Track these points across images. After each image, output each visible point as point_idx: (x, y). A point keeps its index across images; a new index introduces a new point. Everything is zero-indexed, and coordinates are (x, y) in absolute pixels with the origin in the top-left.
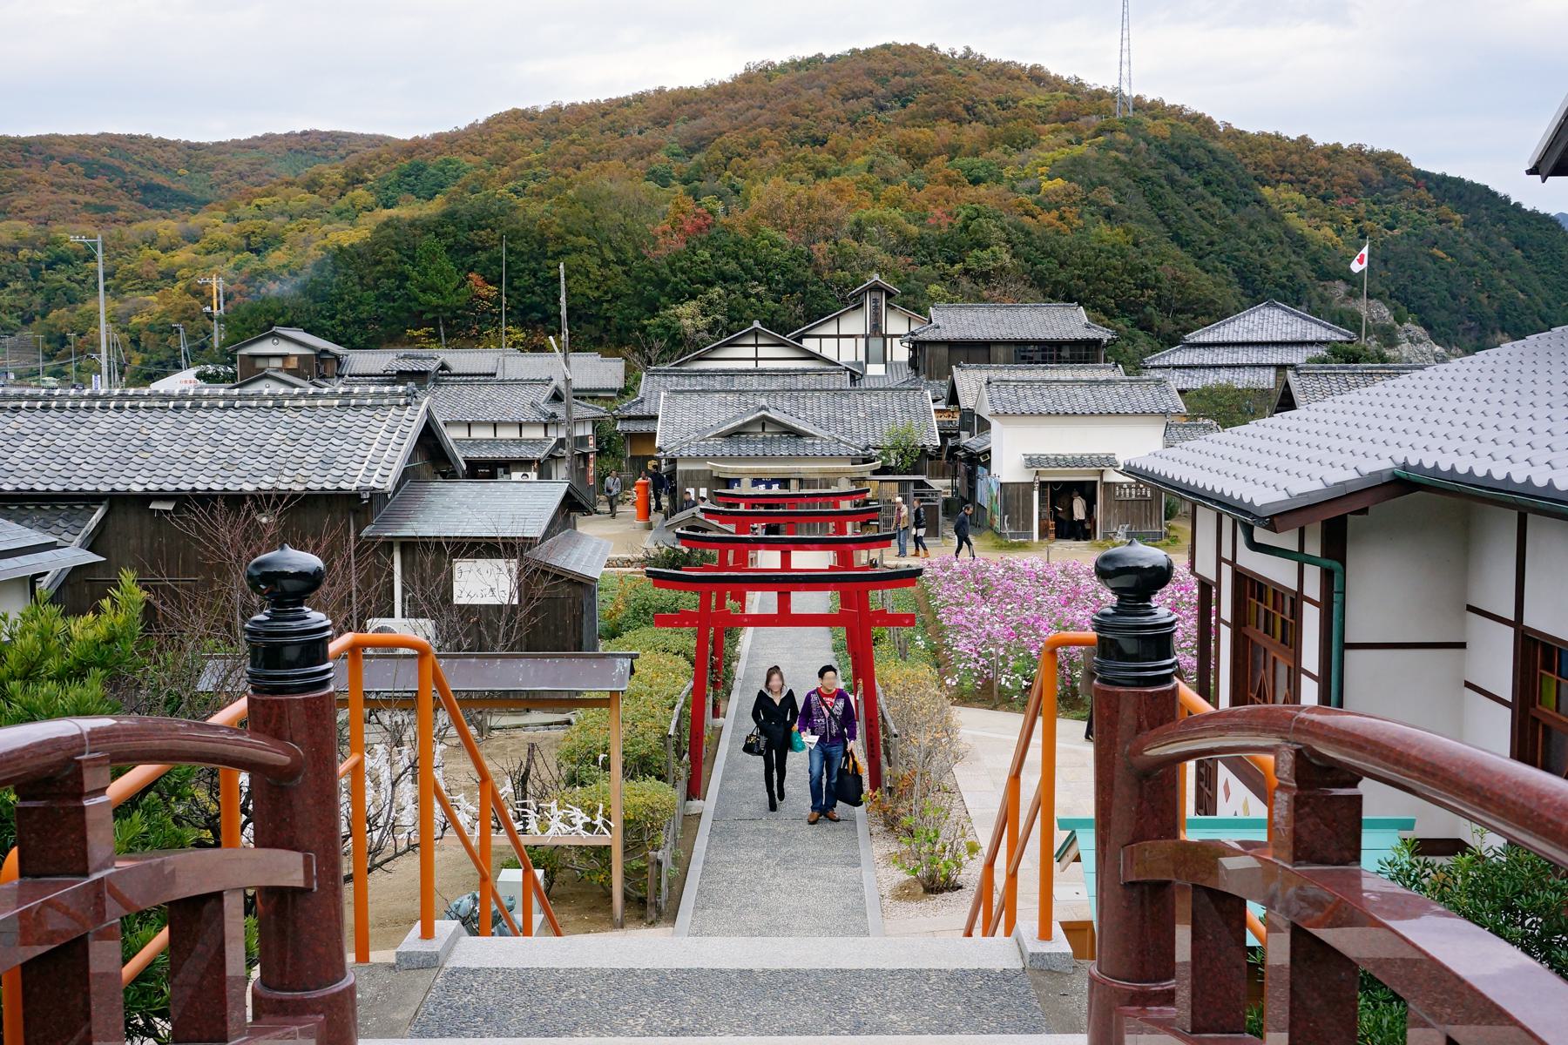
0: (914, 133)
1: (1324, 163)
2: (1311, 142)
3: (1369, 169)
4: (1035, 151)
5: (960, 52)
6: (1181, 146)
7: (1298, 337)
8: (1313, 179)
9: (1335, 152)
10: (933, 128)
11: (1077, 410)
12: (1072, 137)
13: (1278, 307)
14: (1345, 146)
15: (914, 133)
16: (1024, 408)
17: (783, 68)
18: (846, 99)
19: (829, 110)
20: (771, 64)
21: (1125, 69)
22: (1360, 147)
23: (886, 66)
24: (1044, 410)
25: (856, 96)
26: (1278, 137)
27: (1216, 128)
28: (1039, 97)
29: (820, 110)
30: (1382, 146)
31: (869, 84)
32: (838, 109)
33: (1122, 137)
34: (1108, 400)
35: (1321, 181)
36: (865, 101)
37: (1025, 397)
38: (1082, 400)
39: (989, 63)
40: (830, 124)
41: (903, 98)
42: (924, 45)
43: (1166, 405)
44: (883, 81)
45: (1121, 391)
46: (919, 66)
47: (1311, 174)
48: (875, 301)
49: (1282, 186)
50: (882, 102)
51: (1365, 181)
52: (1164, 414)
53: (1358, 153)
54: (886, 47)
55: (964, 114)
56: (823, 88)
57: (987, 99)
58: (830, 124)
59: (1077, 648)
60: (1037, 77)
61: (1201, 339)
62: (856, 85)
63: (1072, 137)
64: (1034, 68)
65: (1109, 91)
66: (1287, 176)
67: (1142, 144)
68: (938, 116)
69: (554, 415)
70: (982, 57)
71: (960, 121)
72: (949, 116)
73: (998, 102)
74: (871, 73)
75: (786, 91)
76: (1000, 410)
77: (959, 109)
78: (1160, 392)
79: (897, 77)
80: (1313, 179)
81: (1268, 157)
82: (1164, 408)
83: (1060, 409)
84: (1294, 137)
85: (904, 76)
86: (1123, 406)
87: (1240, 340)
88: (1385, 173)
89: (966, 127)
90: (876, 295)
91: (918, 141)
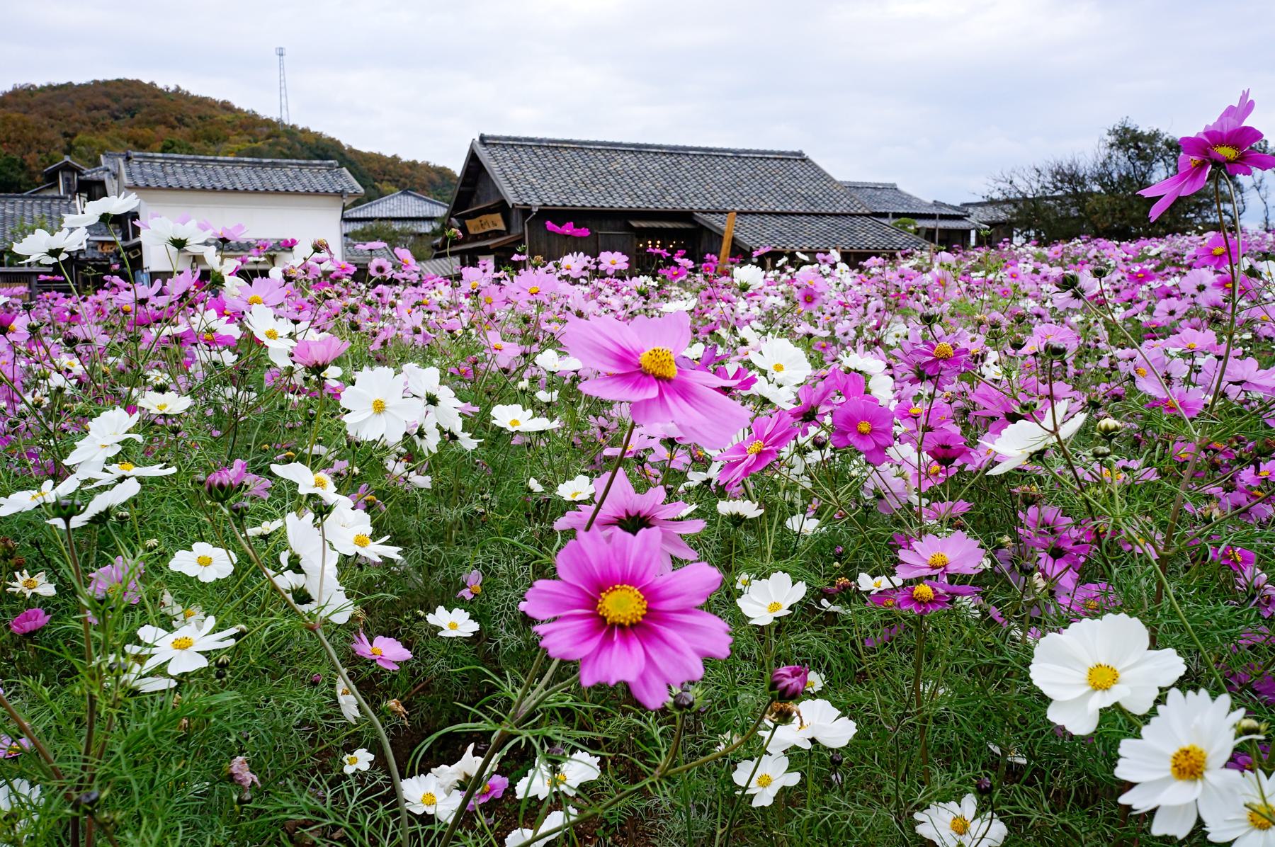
0: (140, 132)
1: (408, 170)
2: (400, 159)
3: (434, 176)
4: (226, 144)
5: (172, 88)
6: (322, 149)
7: (428, 214)
8: (403, 180)
9: (413, 165)
10: (152, 129)
11: (239, 186)
12: (251, 139)
13: (410, 194)
14: (419, 162)
15: (140, 132)
16: (172, 182)
17: (43, 89)
18: (89, 110)
19: (77, 116)
20: (33, 86)
21: (284, 100)
22: (428, 163)
23: (119, 91)
24: (197, 185)
25: (96, 108)
26: (380, 155)
27: (343, 147)
28: (227, 117)
29: (70, 116)
30: (440, 164)
31: (107, 101)
32: (85, 116)
33: (284, 140)
34: (275, 179)
35: (407, 181)
36: (104, 112)
37: (174, 173)
38: (244, 179)
39: (193, 96)
40: (77, 125)
41: (131, 111)
42: (146, 81)
43: (342, 186)
44: (116, 101)
45: (291, 174)
46: (143, 93)
47: (401, 176)
48: (68, 180)
49: (384, 183)
50: (117, 114)
51: (432, 182)
52: (340, 194)
53: (426, 166)
54: (119, 80)
55: (176, 123)
56: (73, 103)
57: (193, 115)
58: (77, 125)
59: (623, 801)
60: (226, 107)
61: (354, 215)
62: (97, 101)
63: (251, 139)
64: (224, 102)
65: (275, 120)
66: (387, 177)
67: (298, 146)
68: (158, 122)
69: (1076, 774)
70: (188, 93)
71: (173, 127)
72: (165, 123)
73: (200, 118)
74: (108, 95)
75: (44, 103)
76: (141, 183)
77: (172, 119)
78: (333, 176)
79: (127, 99)
80: (403, 180)
81: (375, 166)
82: (339, 189)
83: (218, 185)
84: (389, 155)
85: (132, 98)
86: (293, 185)
87: (384, 216)
88: (443, 179)
89: (177, 130)
90: (68, 174)
91: (142, 136)
